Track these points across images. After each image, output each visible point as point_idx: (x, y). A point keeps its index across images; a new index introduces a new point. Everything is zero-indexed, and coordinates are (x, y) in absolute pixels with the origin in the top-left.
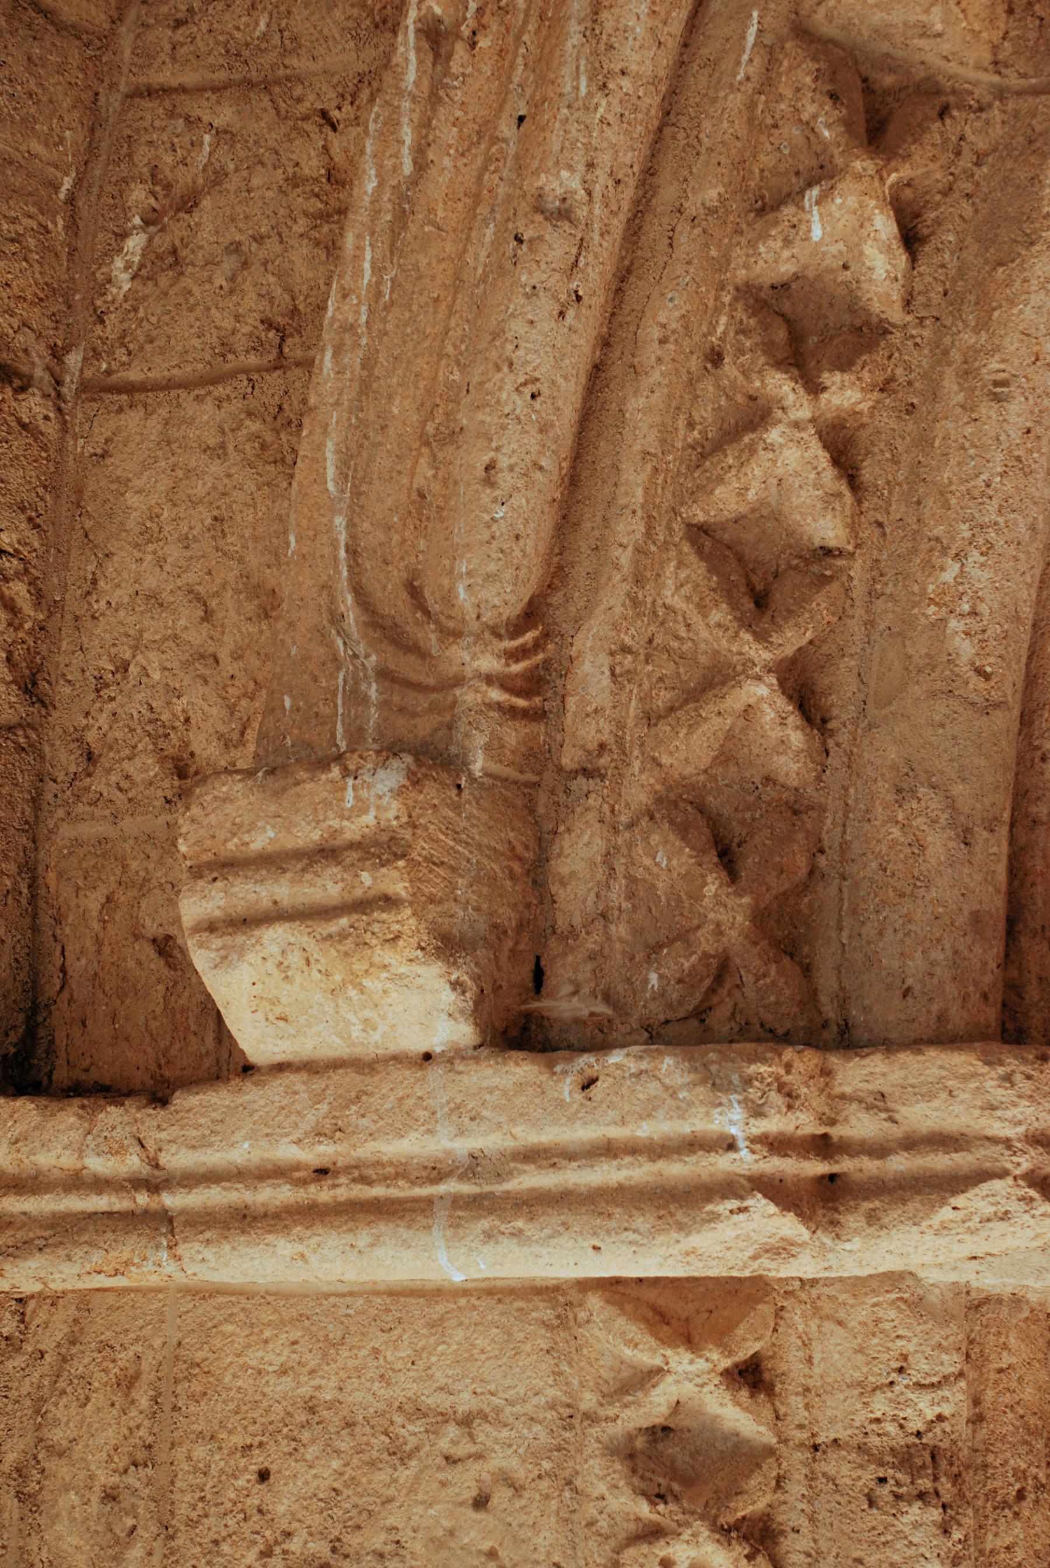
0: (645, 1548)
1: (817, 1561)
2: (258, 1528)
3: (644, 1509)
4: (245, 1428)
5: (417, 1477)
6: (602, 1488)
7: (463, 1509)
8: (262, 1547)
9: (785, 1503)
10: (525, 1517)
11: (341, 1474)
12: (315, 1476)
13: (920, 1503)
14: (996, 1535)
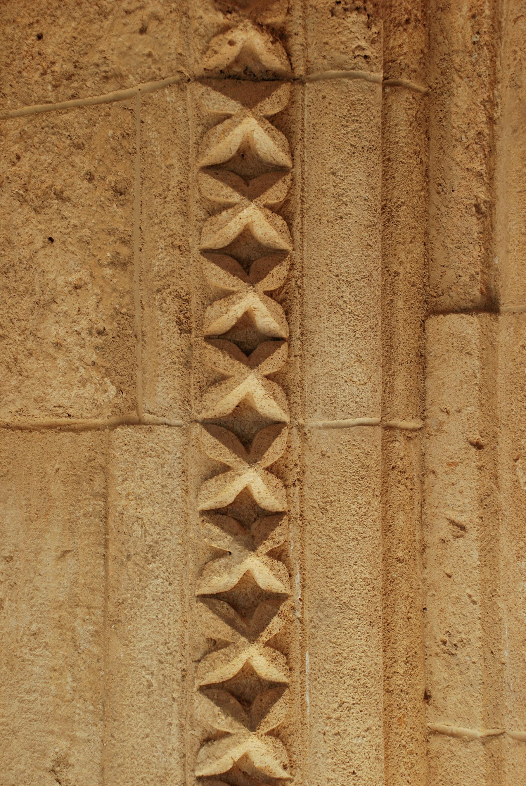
0: (221, 37)
1: (306, 48)
2: (39, 62)
3: (220, 18)
4: (29, 14)
5: (112, 24)
6: (201, 12)
7: (135, 35)
8: (42, 71)
9: (291, 21)
10: (164, 33)
11: (76, 29)
12: (64, 32)
13: (356, 12)
14: (394, 39)
